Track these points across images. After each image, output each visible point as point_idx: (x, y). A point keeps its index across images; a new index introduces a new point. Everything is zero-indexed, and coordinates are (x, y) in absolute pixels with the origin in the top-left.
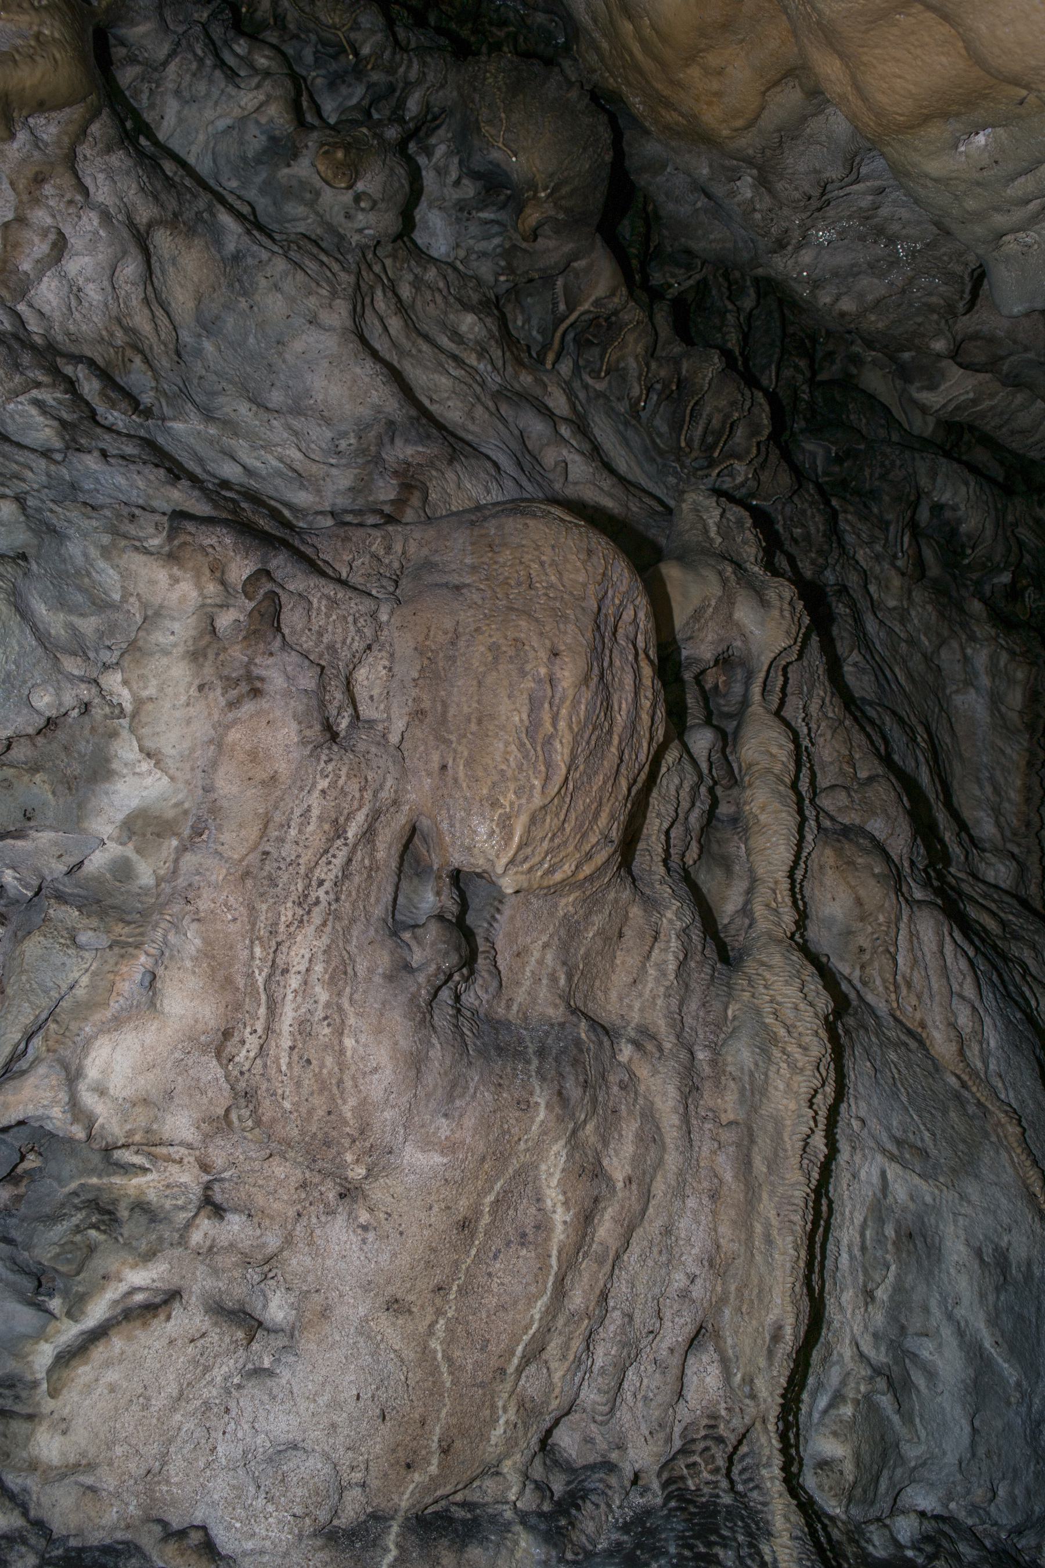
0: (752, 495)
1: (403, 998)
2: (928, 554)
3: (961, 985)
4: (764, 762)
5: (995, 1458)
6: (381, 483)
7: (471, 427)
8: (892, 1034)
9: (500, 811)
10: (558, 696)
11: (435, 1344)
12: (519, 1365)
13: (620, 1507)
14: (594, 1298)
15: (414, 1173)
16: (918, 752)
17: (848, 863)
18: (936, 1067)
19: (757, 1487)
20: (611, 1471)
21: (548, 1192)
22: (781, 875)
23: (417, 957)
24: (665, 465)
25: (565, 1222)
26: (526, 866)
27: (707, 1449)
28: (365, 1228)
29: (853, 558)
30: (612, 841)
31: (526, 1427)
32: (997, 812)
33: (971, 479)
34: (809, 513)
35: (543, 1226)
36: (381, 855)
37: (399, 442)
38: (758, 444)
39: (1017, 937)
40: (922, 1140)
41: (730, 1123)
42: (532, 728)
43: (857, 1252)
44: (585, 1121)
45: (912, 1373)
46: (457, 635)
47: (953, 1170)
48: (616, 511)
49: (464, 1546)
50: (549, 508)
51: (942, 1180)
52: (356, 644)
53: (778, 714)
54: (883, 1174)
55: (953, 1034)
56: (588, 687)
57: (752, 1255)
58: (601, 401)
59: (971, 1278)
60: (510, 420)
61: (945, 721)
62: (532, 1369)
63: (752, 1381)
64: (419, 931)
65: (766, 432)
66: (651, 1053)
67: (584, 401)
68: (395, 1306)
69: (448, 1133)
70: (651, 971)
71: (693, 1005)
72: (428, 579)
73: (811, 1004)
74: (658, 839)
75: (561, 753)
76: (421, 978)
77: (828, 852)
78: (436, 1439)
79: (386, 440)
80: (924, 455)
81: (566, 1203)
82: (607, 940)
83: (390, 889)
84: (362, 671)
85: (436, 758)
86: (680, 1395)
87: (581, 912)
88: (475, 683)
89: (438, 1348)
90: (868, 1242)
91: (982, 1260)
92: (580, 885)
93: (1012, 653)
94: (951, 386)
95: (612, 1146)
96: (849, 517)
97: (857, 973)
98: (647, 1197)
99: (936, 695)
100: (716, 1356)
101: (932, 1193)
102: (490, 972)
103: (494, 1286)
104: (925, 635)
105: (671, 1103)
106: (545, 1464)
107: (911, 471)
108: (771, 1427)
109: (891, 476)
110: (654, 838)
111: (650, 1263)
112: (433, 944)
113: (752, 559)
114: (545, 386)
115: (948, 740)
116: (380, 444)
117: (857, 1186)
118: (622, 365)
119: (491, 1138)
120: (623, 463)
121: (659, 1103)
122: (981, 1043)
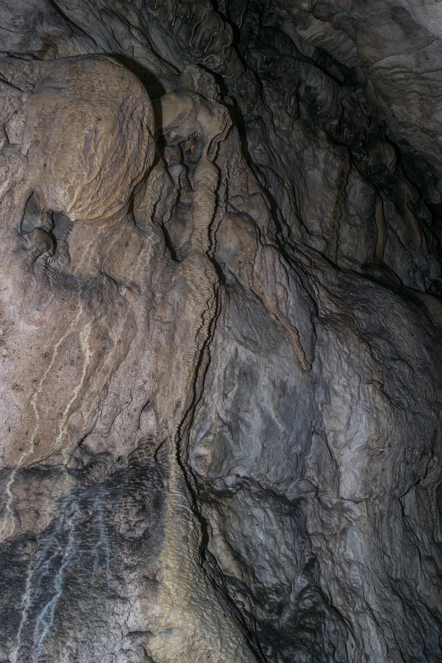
0: (223, 73)
1: (20, 260)
2: (303, 109)
3: (281, 279)
4: (204, 181)
5: (271, 458)
6: (34, 42)
7: (87, 24)
8: (250, 297)
9: (69, 185)
10: (98, 137)
11: (32, 403)
12: (69, 412)
13: (111, 468)
14: (101, 387)
15: (24, 333)
16: (284, 190)
17: (237, 226)
18: (267, 311)
19: (166, 461)
20: (108, 455)
21: (83, 344)
22: (205, 228)
23: (29, 245)
24: (183, 55)
25: (90, 356)
26: (80, 209)
27: (147, 447)
28: (5, 357)
29: (268, 106)
30: (121, 203)
31: (72, 437)
32: (321, 221)
33: (324, 76)
34: (249, 84)
35: (81, 358)
36: (16, 202)
37: (45, 24)
38: (226, 48)
39: (316, 267)
40: (256, 338)
41: (167, 322)
42: (86, 150)
43: (222, 379)
44: (101, 316)
45: (240, 426)
46: (57, 109)
47: (267, 350)
48: (155, 72)
49: (42, 479)
50: (108, 58)
51: (262, 354)
52: (9, 110)
53: (214, 163)
54: (236, 350)
55: (274, 298)
56: (113, 135)
57: (171, 373)
58: (155, 22)
59: (269, 391)
60: (108, 24)
61: (302, 181)
62: (74, 414)
63: (167, 422)
64: (30, 234)
65: (230, 43)
66: (135, 293)
67: (147, 21)
68: (16, 387)
69: (39, 317)
70: (139, 260)
71: (157, 275)
72: (47, 84)
73: (208, 278)
74: (150, 208)
75: (97, 162)
76: (30, 253)
77: (230, 221)
78: (32, 439)
79: (38, 22)
80: (304, 63)
81: (91, 349)
82: (120, 246)
83: (20, 217)
84: (13, 123)
85: (42, 161)
86: (139, 428)
87: (108, 233)
88: (62, 130)
89: (34, 404)
90: (227, 375)
91: (274, 385)
92: (107, 220)
93: (335, 155)
94: (314, 28)
95: (114, 328)
96: (270, 89)
97: (237, 271)
98: (127, 349)
99: (300, 170)
100: (154, 413)
101: (257, 358)
102: (65, 255)
103: (59, 381)
104: (298, 144)
105: (141, 313)
106: (81, 452)
107: (297, 70)
108: (173, 439)
109: (288, 71)
110: (148, 207)
111: (128, 375)
112: (36, 239)
113: (212, 97)
114: (128, 11)
115: (303, 190)
116: (35, 23)
117: (224, 353)
118: (165, 4)
119: (58, 320)
120: (164, 52)
121: (136, 312)
122: (286, 302)
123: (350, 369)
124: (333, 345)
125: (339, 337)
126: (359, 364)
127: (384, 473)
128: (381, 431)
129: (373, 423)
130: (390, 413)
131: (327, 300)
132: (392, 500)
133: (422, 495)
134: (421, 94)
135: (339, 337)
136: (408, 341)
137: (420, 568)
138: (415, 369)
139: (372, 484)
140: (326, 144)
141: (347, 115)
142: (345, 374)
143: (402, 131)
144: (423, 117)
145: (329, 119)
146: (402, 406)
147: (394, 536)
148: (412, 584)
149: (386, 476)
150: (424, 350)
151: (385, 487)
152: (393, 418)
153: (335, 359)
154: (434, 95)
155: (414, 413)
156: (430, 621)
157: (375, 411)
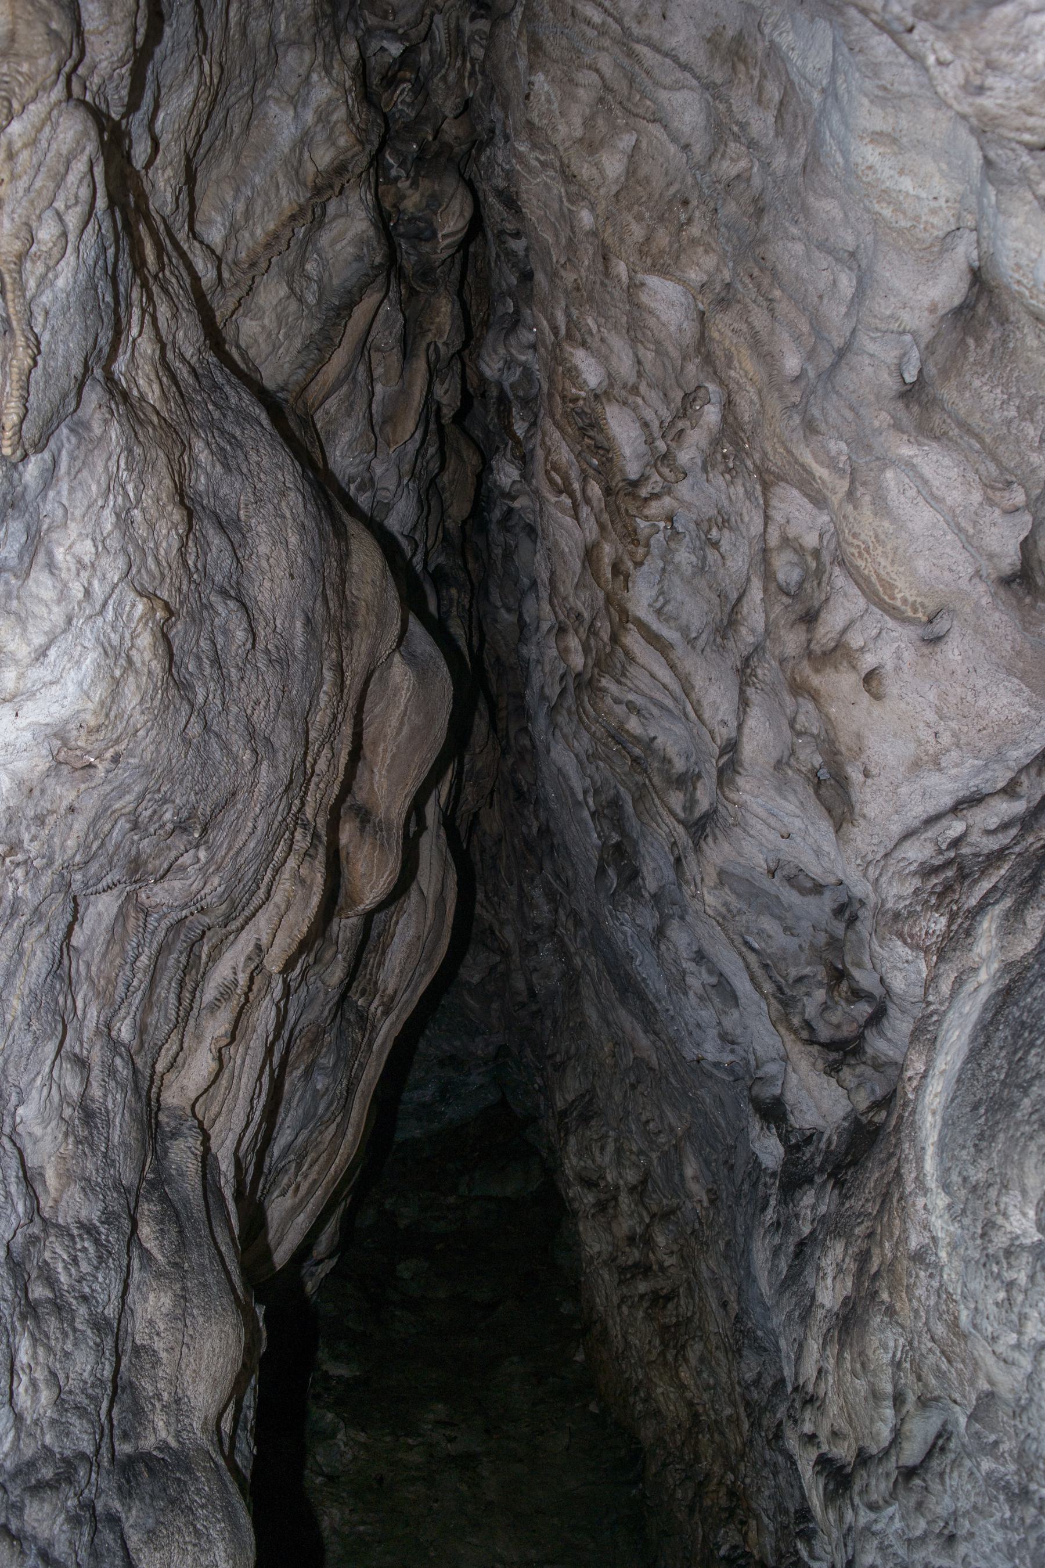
32: (233, 231)
61: (245, 109)
93: (351, 117)
104: (287, 18)
115: (237, 130)
122: (48, 269)
123: (116, 534)
124: (105, 456)
125: (130, 451)
126: (144, 542)
127: (70, 817)
128: (112, 714)
129: (104, 684)
130: (156, 689)
131: (148, 368)
132: (56, 888)
133: (131, 923)
134: (606, 88)
135: (130, 451)
136: (277, 580)
137: (47, 1070)
138: (260, 646)
139: (28, 827)
140: (346, 77)
141: (428, 58)
142: (99, 537)
143: (522, 149)
144: (581, 140)
145: (389, 30)
146: (191, 696)
147: (21, 971)
148: (10, 1096)
149: (71, 828)
150: (299, 624)
151: (57, 849)
152: (156, 703)
153: (94, 488)
154: (629, 105)
155: (206, 727)
156: (13, 1189)
157: (122, 662)
